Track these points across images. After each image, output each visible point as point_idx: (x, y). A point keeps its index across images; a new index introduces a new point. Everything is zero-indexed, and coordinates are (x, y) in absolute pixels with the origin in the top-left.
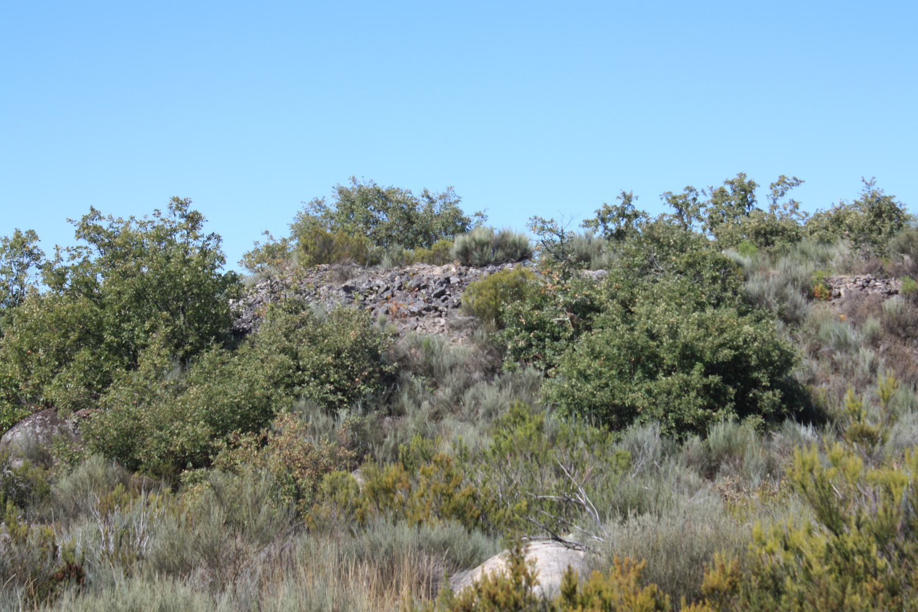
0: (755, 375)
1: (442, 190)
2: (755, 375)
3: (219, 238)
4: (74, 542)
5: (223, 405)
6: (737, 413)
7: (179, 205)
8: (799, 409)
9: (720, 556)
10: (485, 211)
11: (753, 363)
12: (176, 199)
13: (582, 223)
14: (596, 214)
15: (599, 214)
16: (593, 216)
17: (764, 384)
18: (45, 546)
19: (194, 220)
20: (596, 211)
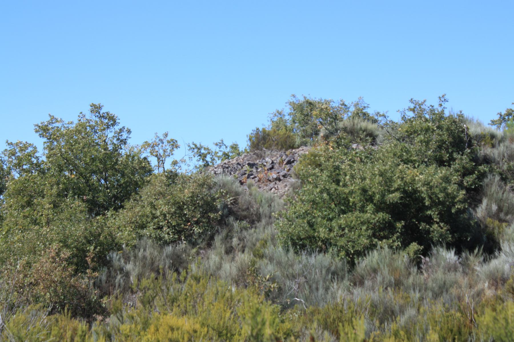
0: (429, 212)
1: (355, 100)
2: (429, 212)
3: (129, 132)
4: (348, 276)
5: (319, 232)
6: (401, 242)
7: (96, 109)
8: (467, 239)
9: (393, 326)
10: (386, 113)
11: (427, 204)
12: (93, 105)
13: (490, 122)
14: (499, 116)
15: (501, 115)
16: (497, 118)
17: (471, 222)
18: (262, 282)
19: (112, 120)
20: (498, 114)
